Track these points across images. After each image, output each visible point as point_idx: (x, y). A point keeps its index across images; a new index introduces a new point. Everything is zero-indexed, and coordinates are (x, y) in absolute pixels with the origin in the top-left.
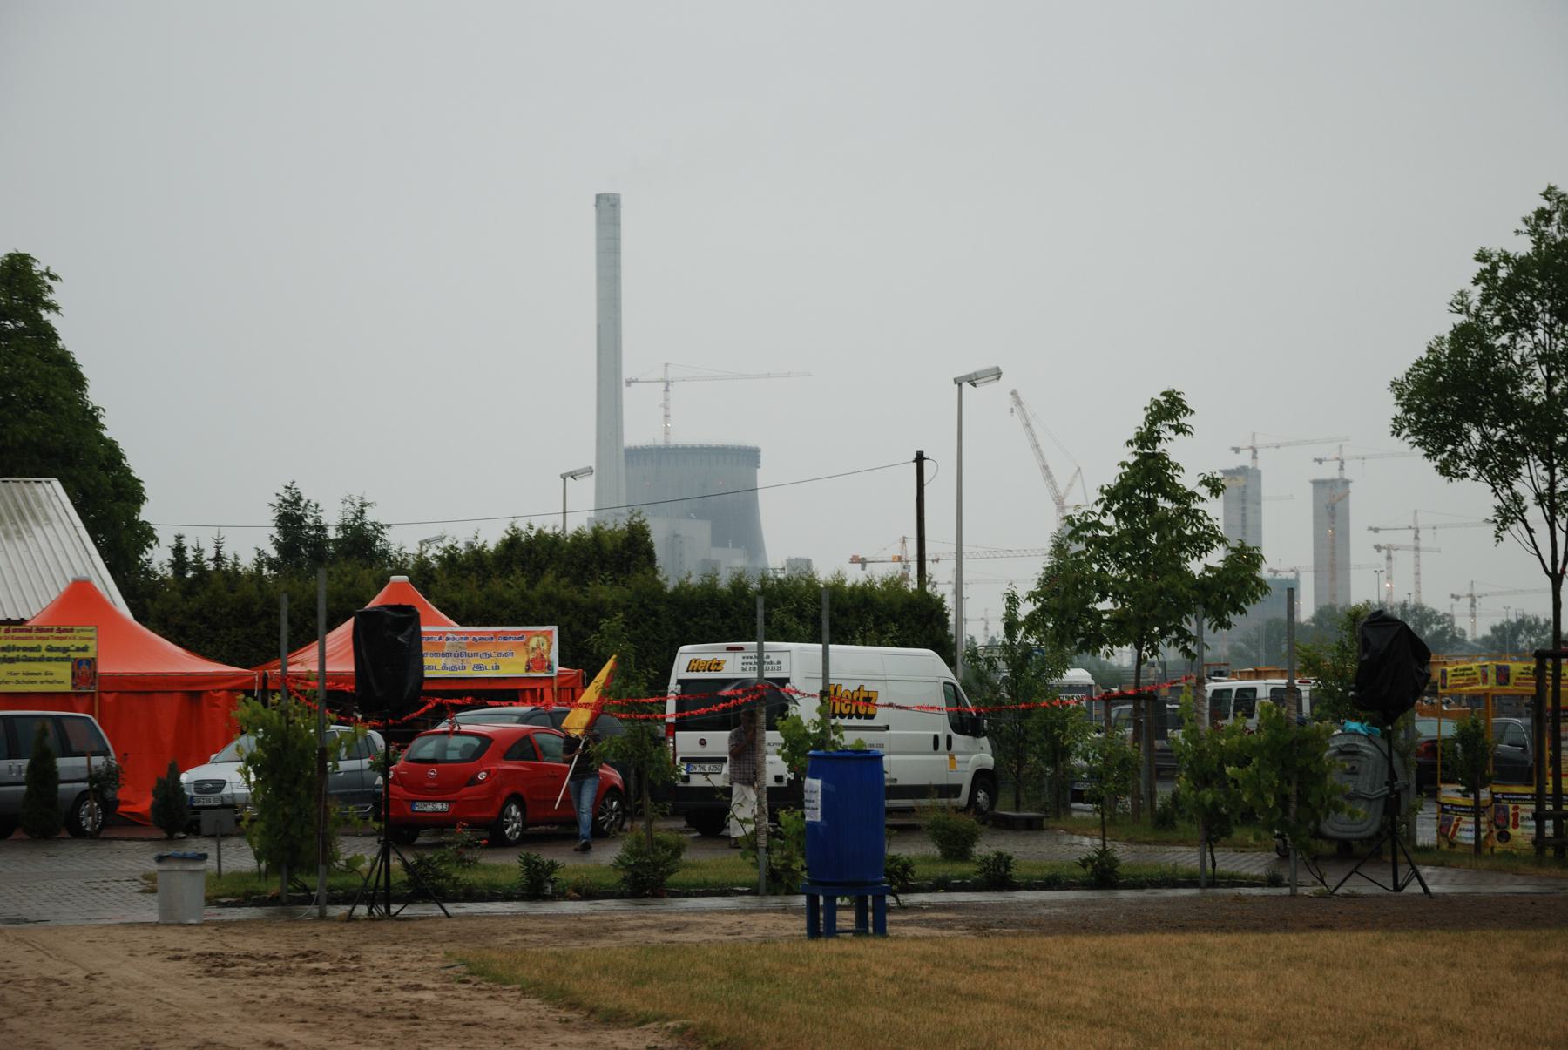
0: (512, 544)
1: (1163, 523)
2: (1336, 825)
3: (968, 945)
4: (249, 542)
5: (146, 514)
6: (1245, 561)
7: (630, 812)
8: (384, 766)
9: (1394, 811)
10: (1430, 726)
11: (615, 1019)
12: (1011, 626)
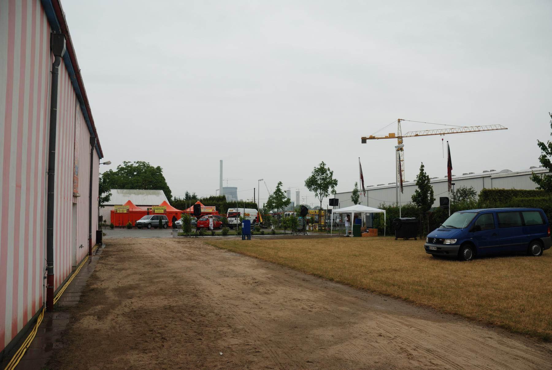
0: (163, 177)
1: (280, 196)
2: (298, 228)
3: (260, 241)
4: (182, 197)
5: (171, 194)
6: (289, 200)
7: (223, 226)
8: (197, 221)
9: (304, 226)
10: (308, 217)
11: (221, 248)
12: (264, 207)
